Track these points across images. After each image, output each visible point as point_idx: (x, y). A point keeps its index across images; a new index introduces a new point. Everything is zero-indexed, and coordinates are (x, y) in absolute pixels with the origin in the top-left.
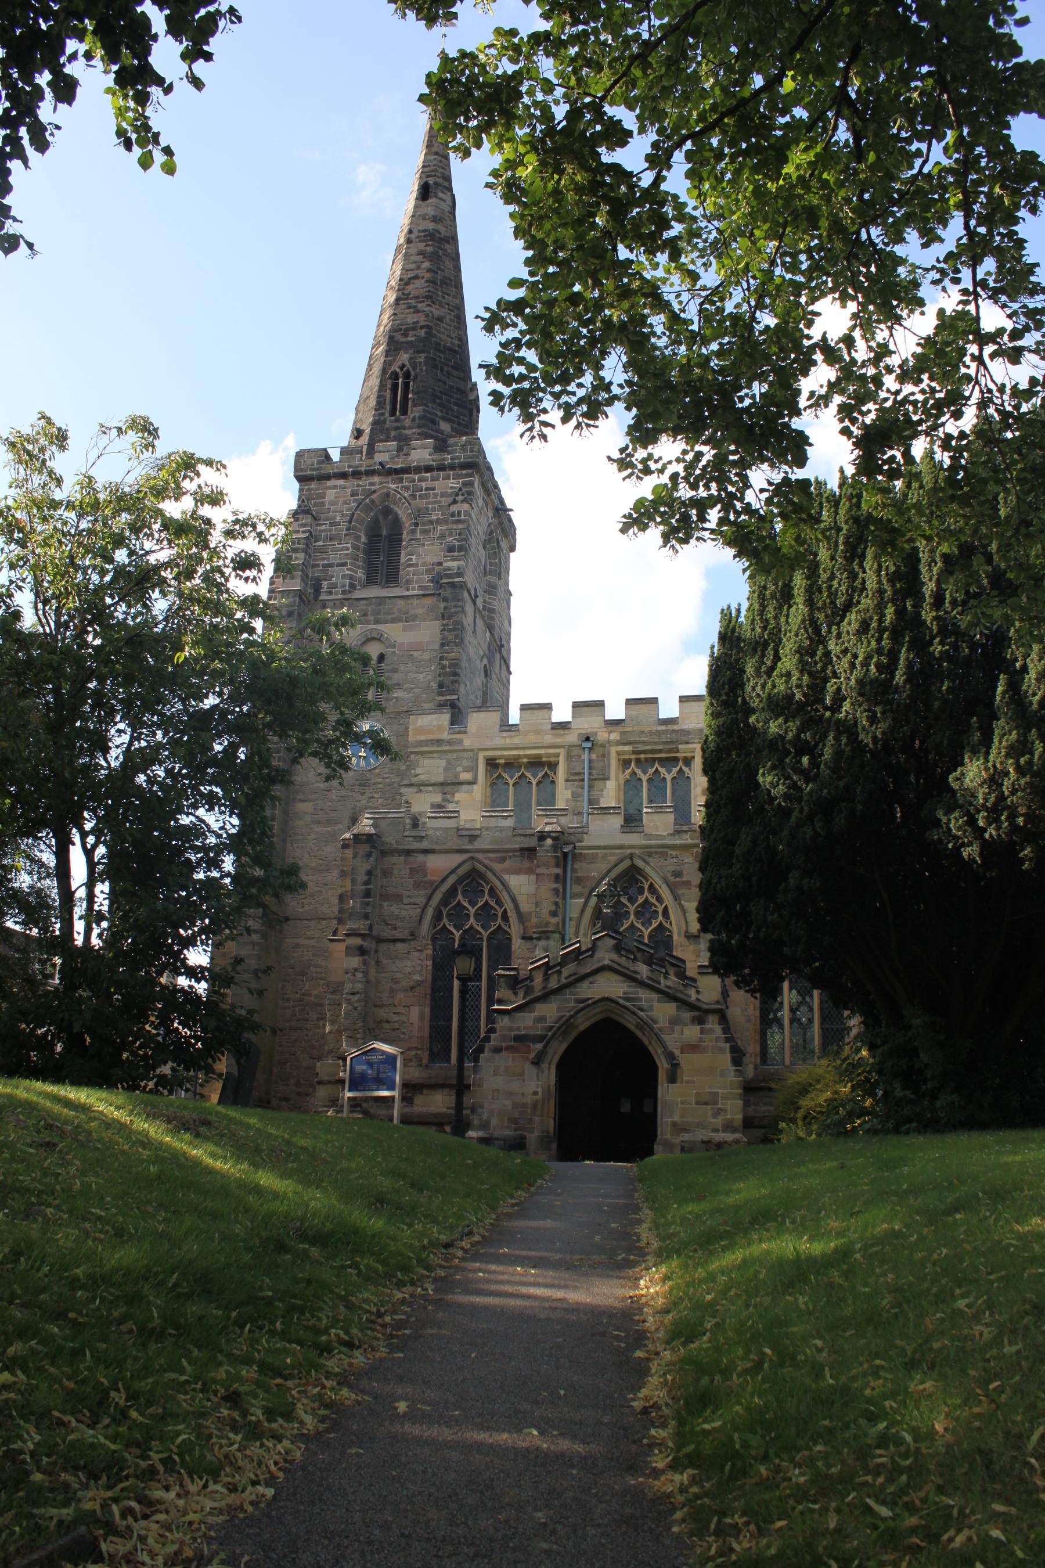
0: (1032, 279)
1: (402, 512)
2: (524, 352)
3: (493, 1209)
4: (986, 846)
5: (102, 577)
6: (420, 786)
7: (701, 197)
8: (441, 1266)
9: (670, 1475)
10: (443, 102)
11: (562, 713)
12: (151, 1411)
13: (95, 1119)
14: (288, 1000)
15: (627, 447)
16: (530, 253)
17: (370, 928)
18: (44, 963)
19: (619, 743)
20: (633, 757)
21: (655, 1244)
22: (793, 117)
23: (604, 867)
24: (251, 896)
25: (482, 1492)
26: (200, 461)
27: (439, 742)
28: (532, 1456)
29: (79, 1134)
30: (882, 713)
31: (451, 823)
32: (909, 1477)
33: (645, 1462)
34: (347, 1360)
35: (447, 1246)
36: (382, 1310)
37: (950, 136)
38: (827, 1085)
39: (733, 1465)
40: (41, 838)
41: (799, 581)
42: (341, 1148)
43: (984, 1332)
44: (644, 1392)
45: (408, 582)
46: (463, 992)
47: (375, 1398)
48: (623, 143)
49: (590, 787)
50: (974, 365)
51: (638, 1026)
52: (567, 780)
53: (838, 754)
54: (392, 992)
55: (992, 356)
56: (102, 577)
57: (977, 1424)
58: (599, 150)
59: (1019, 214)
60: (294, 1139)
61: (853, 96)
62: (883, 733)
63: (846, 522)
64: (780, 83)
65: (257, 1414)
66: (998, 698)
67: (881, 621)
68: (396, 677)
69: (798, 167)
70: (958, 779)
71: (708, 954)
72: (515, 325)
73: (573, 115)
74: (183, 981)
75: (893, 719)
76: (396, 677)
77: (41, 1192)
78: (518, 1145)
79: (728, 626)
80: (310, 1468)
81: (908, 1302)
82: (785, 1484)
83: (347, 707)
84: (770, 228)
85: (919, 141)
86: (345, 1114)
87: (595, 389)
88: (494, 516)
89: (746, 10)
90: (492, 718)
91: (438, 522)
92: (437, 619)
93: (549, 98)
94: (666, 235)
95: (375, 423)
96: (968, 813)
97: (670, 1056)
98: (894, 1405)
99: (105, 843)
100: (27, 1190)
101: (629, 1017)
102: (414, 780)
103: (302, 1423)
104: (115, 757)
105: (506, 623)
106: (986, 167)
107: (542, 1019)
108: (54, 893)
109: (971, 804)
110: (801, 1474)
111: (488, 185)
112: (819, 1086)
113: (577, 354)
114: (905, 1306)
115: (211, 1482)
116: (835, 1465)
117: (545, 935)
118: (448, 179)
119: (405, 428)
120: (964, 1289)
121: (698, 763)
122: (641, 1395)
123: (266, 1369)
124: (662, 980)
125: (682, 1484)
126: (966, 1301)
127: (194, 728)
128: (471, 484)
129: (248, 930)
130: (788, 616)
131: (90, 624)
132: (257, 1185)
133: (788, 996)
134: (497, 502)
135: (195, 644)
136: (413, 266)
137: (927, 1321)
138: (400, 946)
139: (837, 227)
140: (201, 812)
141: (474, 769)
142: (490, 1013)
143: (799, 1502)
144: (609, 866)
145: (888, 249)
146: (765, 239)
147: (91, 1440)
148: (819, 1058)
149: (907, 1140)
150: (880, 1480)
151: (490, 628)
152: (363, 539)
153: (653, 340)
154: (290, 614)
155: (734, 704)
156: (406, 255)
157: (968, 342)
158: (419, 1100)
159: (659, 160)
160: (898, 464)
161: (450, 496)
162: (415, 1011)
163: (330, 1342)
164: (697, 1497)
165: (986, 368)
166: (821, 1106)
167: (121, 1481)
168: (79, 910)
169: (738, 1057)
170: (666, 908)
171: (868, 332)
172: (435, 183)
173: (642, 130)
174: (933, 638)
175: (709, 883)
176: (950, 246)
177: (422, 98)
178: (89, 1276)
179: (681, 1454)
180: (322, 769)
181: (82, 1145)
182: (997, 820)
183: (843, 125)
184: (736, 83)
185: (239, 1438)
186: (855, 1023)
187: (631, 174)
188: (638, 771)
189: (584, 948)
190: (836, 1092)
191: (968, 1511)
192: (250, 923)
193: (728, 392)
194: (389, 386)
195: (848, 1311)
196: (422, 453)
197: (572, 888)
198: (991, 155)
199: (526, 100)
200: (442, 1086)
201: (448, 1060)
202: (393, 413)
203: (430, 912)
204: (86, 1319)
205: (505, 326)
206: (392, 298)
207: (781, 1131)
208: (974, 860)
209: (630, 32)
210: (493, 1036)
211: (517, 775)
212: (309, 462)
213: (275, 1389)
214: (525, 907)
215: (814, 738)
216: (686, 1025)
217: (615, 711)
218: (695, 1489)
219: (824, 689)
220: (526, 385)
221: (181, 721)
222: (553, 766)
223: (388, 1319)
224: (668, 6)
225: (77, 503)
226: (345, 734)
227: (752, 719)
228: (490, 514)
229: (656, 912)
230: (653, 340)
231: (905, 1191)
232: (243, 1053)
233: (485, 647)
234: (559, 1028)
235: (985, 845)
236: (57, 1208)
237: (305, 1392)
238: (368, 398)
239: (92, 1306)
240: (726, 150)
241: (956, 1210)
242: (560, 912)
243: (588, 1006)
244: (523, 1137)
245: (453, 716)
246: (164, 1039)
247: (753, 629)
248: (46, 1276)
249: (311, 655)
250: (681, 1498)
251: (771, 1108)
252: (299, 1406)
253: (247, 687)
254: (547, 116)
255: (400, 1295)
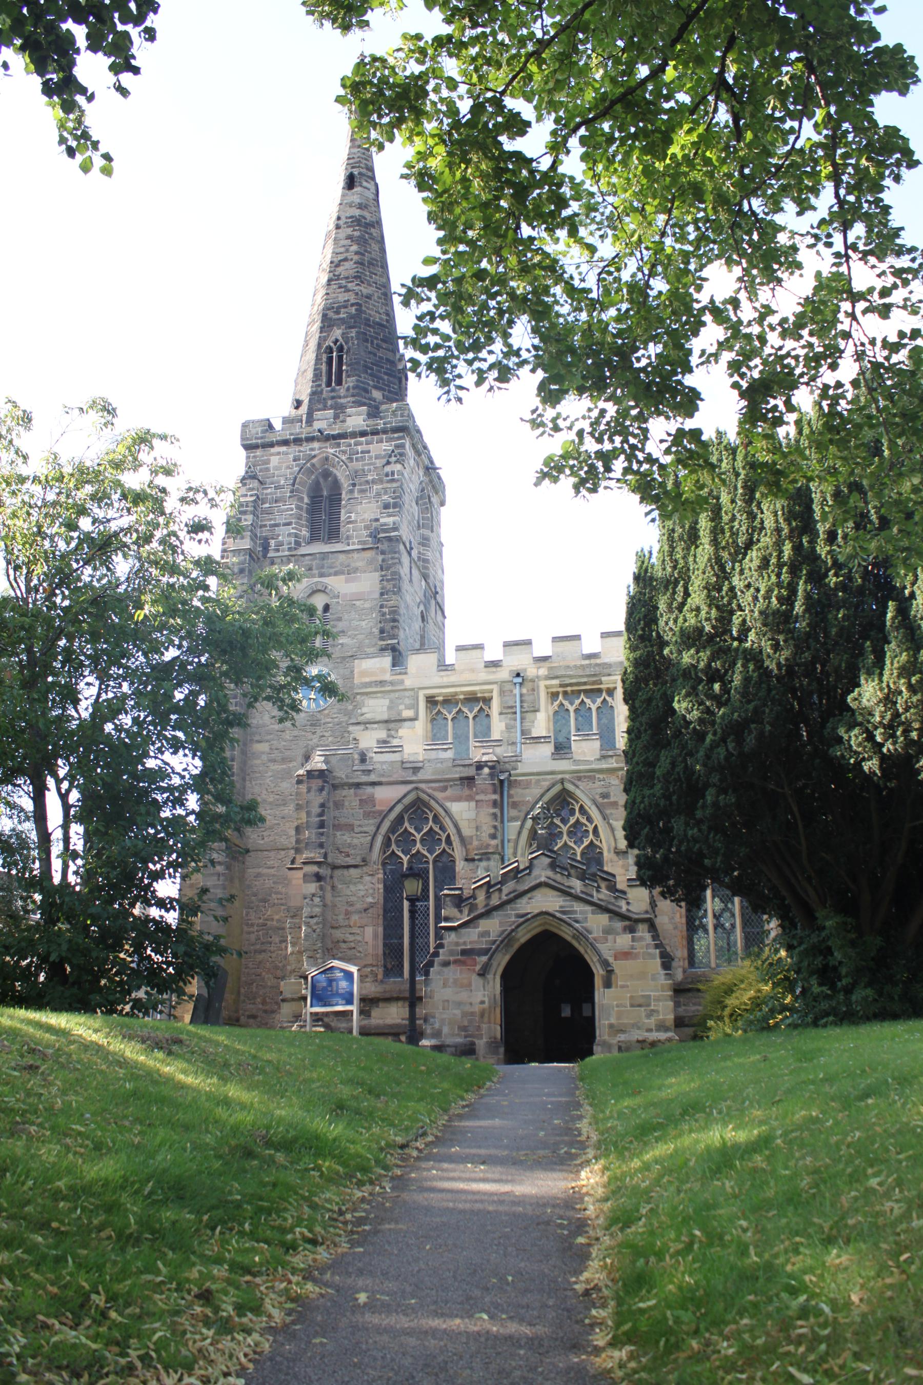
0: (898, 241)
1: (341, 474)
2: (438, 324)
3: (446, 1111)
4: (884, 759)
5: (68, 544)
6: (367, 724)
7: (596, 177)
8: (398, 1166)
9: (610, 1352)
10: (357, 102)
11: (493, 652)
12: (128, 1311)
13: (74, 1042)
14: (252, 925)
15: (537, 409)
16: (441, 234)
17: (325, 856)
18: (24, 899)
19: (548, 678)
20: (561, 690)
21: (594, 1137)
22: (677, 102)
23: (537, 792)
24: (214, 831)
25: (436, 1375)
26: (154, 436)
27: (382, 683)
28: (483, 1339)
29: (60, 1056)
30: (785, 641)
31: (396, 757)
32: (828, 1346)
33: (588, 1341)
34: (311, 1257)
35: (402, 1147)
36: (344, 1208)
37: (819, 115)
38: (750, 984)
39: (667, 1340)
40: (19, 786)
41: (704, 523)
42: (303, 1060)
43: (893, 1207)
44: (586, 1275)
45: (348, 538)
46: (412, 912)
47: (338, 1291)
48: (522, 133)
49: (522, 719)
50: (847, 321)
51: (574, 937)
52: (501, 714)
53: (747, 680)
54: (347, 913)
55: (864, 312)
56: (68, 544)
57: (889, 1293)
58: (500, 138)
59: (884, 183)
60: (259, 1054)
61: (731, 81)
62: (787, 659)
63: (744, 468)
64: (664, 71)
65: (228, 1310)
66: (888, 623)
67: (779, 557)
68: (341, 626)
69: (683, 147)
70: (856, 699)
71: (635, 868)
72: (429, 299)
73: (477, 109)
74: (154, 912)
75: (795, 646)
76: (341, 626)
77: (25, 1111)
78: (468, 1051)
79: (641, 567)
80: (278, 1359)
81: (825, 1182)
82: (715, 1356)
83: (296, 654)
84: (660, 204)
85: (792, 120)
86: (308, 1029)
87: (506, 355)
88: (425, 474)
89: (629, 8)
90: (430, 659)
91: (374, 482)
92: (376, 570)
93: (454, 95)
94: (566, 213)
95: (313, 394)
96: (867, 731)
97: (605, 963)
98: (814, 1279)
99: (77, 787)
100: (12, 1110)
101: (565, 928)
102: (361, 719)
103: (270, 1316)
104: (85, 710)
105: (440, 572)
106: (853, 142)
107: (486, 933)
108: (34, 836)
109: (869, 722)
110: (729, 1346)
111: (404, 177)
112: (742, 986)
113: (486, 324)
114: (822, 1187)
115: (186, 1376)
116: (760, 1337)
117: (485, 856)
118: (371, 169)
119: (340, 397)
120: (875, 1169)
121: (619, 693)
122: (582, 1278)
123: (235, 1267)
124: (595, 894)
125: (621, 1360)
126: (878, 1180)
127: (156, 679)
128: (402, 446)
129: (213, 862)
130: (695, 556)
131: (59, 586)
132: (226, 1097)
133: (711, 903)
134: (427, 462)
135: (154, 602)
136: (342, 250)
137: (843, 1199)
138: (352, 871)
139: (722, 199)
140: (167, 756)
141: (415, 706)
142: (438, 930)
143: (727, 1372)
144: (542, 791)
145: (769, 218)
146: (655, 213)
147: (73, 1341)
148: (742, 959)
149: (824, 1033)
150: (802, 1349)
151: (425, 577)
152: (306, 500)
153: (557, 308)
154: (242, 571)
155: (649, 639)
156: (335, 239)
157: (842, 300)
158: (375, 1012)
159: (557, 147)
160: (781, 412)
161: (384, 457)
162: (369, 931)
163: (295, 1240)
164: (635, 1371)
165: (858, 323)
166: (746, 1004)
167: (102, 1378)
168: (57, 849)
169: (667, 961)
170: (596, 827)
171: (753, 295)
172: (360, 174)
173: (539, 119)
174: (828, 570)
175: (634, 802)
176: (823, 213)
177: (339, 100)
178: (71, 1188)
179: (620, 1332)
180: (276, 712)
181: (63, 1066)
182: (893, 736)
183: (722, 107)
184: (623, 74)
185: (211, 1333)
186: (773, 926)
187: (531, 160)
188: (566, 703)
189: (522, 867)
190: (759, 991)
191: (882, 1375)
192: (215, 856)
193: (626, 353)
194: (324, 359)
195: (770, 1193)
196: (356, 419)
197: (509, 812)
198: (857, 130)
199: (433, 96)
200: (398, 999)
201: (401, 975)
202: (329, 384)
203: (379, 840)
204: (68, 1228)
205: (420, 300)
206: (324, 278)
207: (709, 1029)
208: (874, 773)
209: (525, 31)
210: (441, 951)
211: (455, 711)
212: (254, 431)
213: (244, 1286)
214: (467, 831)
215: (723, 666)
216: (618, 934)
217: (543, 648)
218: (633, 1365)
219: (730, 621)
220: (441, 353)
221: (144, 674)
222: (487, 701)
223: (348, 1216)
224: (560, 9)
225: (43, 478)
226: (296, 679)
227: (666, 652)
228: (421, 473)
229: (587, 831)
230: (557, 308)
231: (821, 1080)
232: (212, 975)
233: (421, 594)
234: (502, 942)
235: (883, 759)
236: (40, 1125)
237: (273, 1287)
238: (305, 371)
239: (74, 1216)
240: (617, 135)
241: (868, 1096)
242: (499, 835)
243: (528, 920)
244: (473, 1044)
245: (394, 659)
246: (138, 965)
247: (664, 569)
248: (31, 1189)
249: (262, 608)
250: (620, 1374)
251: (700, 1008)
252: (267, 1300)
253: (204, 639)
254: (453, 111)
255: (360, 1194)
